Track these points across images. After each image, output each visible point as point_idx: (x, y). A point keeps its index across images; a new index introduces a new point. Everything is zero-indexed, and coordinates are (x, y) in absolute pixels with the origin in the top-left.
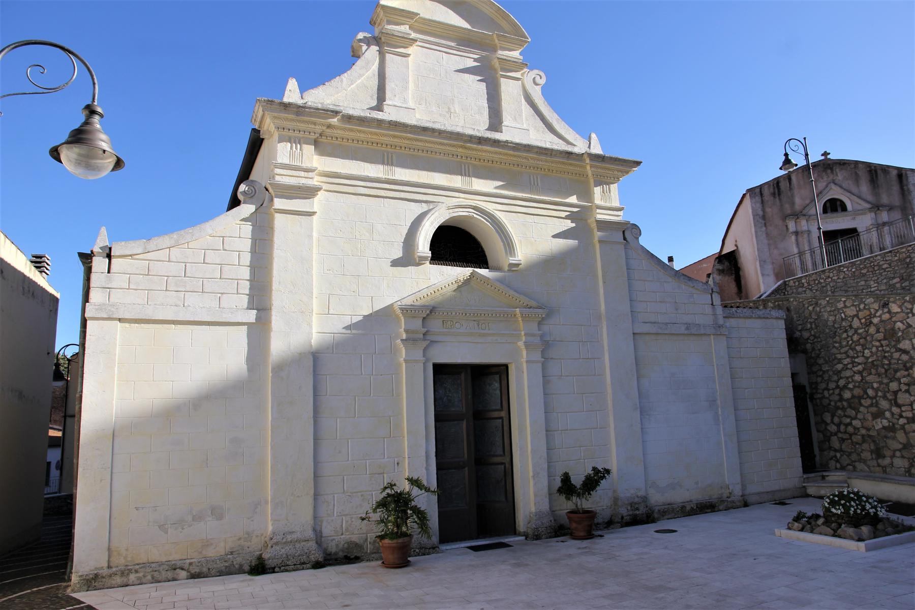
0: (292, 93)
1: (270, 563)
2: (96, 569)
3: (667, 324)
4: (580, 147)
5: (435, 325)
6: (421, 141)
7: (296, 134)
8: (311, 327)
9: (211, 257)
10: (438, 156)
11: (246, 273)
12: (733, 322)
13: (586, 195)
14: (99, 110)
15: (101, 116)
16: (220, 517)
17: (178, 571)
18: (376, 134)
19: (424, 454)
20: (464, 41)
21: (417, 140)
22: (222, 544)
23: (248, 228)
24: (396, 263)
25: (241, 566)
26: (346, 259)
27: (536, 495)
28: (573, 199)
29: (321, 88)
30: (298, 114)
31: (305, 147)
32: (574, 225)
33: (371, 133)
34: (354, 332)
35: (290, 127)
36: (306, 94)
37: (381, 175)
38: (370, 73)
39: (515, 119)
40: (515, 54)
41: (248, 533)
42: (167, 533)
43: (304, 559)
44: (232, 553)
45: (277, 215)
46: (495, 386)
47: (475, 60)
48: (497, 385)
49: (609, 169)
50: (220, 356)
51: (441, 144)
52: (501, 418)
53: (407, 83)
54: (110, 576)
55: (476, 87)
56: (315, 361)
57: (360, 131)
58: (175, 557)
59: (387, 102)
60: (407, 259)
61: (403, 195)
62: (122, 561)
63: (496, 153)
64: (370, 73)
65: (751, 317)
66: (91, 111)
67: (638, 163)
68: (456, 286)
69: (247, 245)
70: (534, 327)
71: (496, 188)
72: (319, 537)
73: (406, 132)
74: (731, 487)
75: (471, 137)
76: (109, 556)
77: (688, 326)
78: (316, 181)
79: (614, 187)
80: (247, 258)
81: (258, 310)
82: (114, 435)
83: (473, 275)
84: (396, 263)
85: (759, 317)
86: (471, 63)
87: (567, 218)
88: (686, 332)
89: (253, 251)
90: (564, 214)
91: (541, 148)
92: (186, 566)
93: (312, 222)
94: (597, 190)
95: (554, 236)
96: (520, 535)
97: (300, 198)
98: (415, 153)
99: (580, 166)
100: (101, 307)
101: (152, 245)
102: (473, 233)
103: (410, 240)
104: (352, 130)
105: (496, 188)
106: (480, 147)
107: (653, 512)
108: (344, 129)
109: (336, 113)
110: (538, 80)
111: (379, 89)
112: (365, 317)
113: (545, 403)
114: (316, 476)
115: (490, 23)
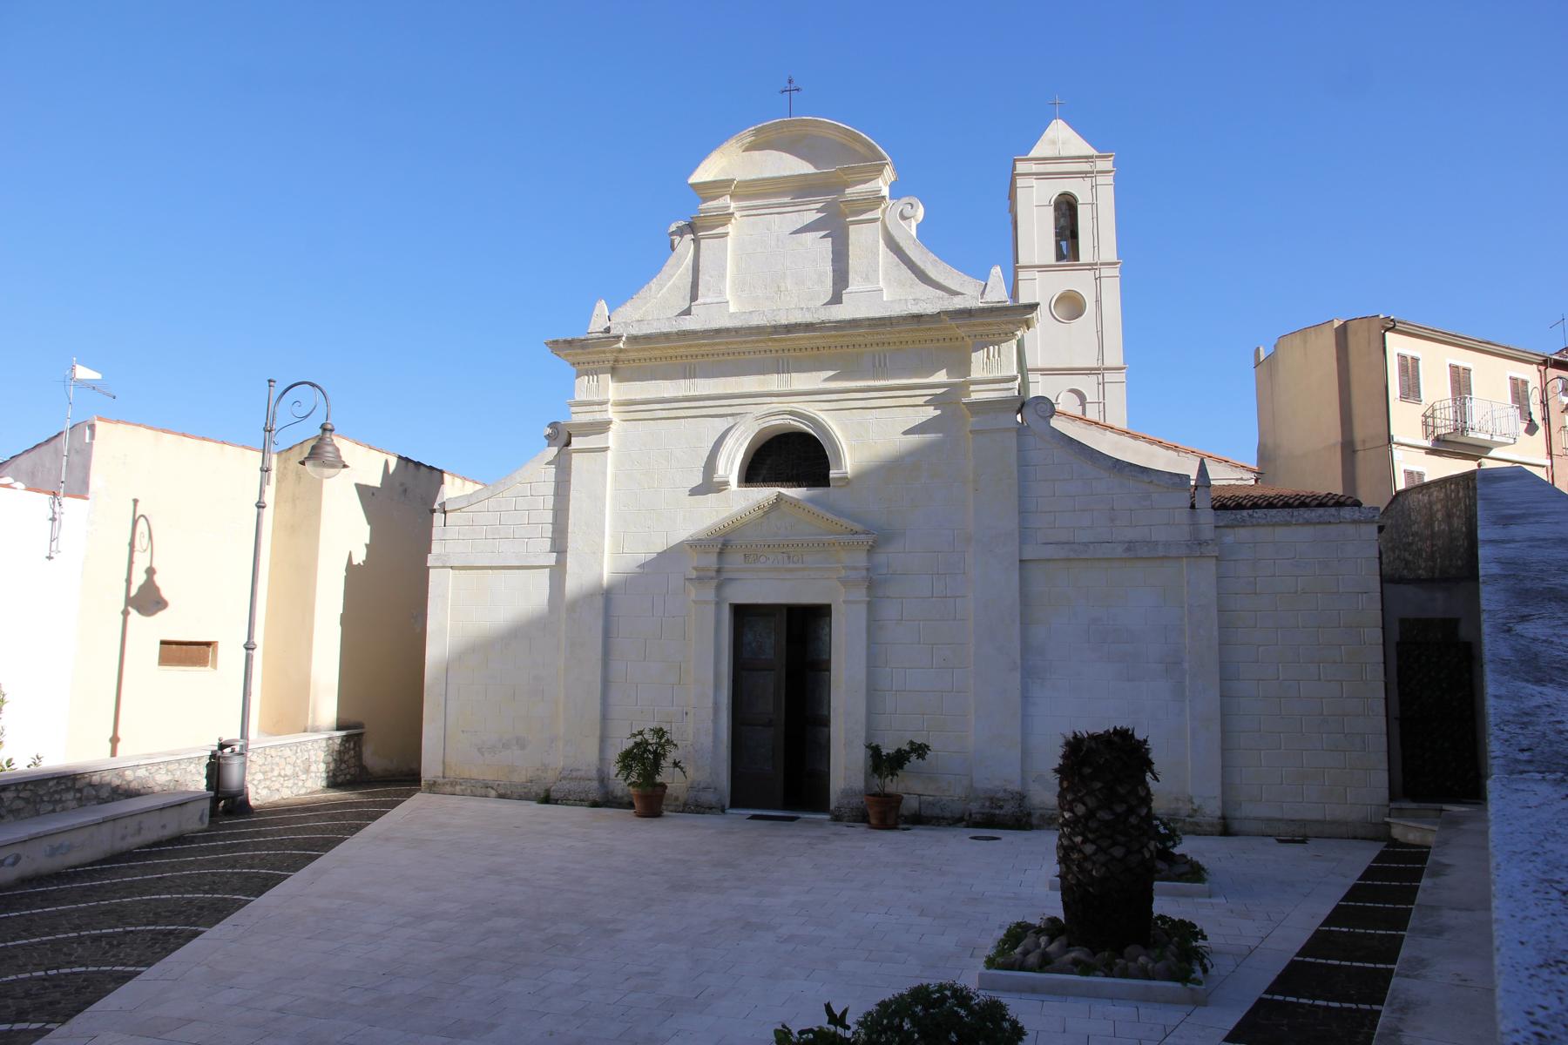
0: (600, 318)
1: (554, 795)
3: (1085, 544)
5: (735, 560)
10: (747, 356)
12: (1230, 537)
13: (963, 366)
16: (523, 747)
20: (800, 189)
23: (552, 470)
24: (694, 492)
26: (654, 487)
28: (941, 377)
37: (681, 393)
39: (867, 279)
47: (819, 211)
50: (526, 596)
55: (819, 247)
56: (607, 598)
58: (489, 776)
59: (700, 301)
60: (709, 485)
65: (1288, 524)
70: (860, 559)
71: (827, 380)
72: (603, 779)
74: (1197, 802)
77: (1130, 546)
82: (447, 669)
83: (780, 497)
84: (694, 492)
85: (1308, 523)
86: (812, 216)
87: (927, 404)
89: (556, 494)
90: (921, 401)
94: (978, 358)
95: (905, 433)
99: (946, 329)
103: (710, 465)
105: (827, 380)
107: (1029, 815)
108: (637, 350)
110: (908, 211)
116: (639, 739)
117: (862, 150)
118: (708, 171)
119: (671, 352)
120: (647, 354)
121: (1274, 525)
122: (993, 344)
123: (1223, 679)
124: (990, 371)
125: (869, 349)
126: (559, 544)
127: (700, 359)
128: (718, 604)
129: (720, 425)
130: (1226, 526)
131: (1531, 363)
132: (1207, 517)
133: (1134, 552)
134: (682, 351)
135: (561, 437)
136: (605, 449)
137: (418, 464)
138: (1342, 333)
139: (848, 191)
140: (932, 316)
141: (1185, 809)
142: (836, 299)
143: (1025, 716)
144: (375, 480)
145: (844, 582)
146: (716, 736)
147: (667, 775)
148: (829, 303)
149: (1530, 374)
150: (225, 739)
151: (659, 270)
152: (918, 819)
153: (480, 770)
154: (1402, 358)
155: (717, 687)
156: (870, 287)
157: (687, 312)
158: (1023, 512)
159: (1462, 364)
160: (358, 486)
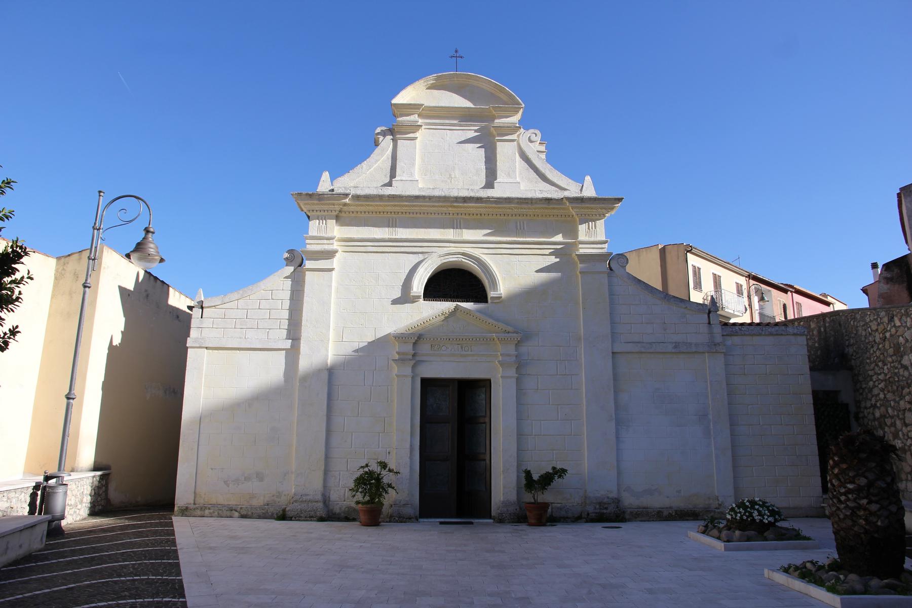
0: (325, 184)
1: (289, 514)
3: (651, 343)
4: (573, 190)
5: (424, 348)
7: (322, 213)
8: (327, 351)
9: (264, 304)
10: (433, 216)
11: (286, 314)
12: (730, 341)
13: (574, 233)
14: (152, 230)
15: (153, 233)
19: (408, 446)
20: (465, 117)
23: (289, 282)
24: (395, 302)
25: (273, 514)
26: (361, 299)
27: (504, 487)
28: (559, 238)
29: (346, 175)
30: (320, 199)
32: (558, 260)
37: (386, 236)
39: (509, 175)
40: (515, 119)
43: (312, 513)
47: (476, 131)
48: (483, 396)
50: (267, 371)
51: (434, 206)
52: (485, 423)
55: (477, 153)
56: (330, 374)
57: (368, 205)
58: (233, 502)
60: (405, 298)
61: (403, 249)
63: (482, 207)
65: (760, 335)
67: (620, 200)
68: (443, 317)
69: (288, 294)
70: (511, 349)
71: (485, 235)
72: (326, 501)
75: (456, 198)
77: (676, 345)
78: (336, 246)
79: (601, 223)
80: (287, 304)
83: (457, 308)
84: (395, 302)
85: (771, 334)
87: (551, 254)
89: (292, 299)
91: (521, 199)
93: (331, 278)
94: (582, 228)
95: (537, 271)
96: (490, 517)
98: (415, 215)
99: (564, 209)
100: (196, 340)
101: (227, 300)
104: (362, 205)
105: (485, 235)
107: (624, 512)
108: (357, 205)
109: (347, 195)
110: (533, 138)
112: (369, 343)
113: (518, 412)
114: (327, 457)
115: (491, 97)
116: (366, 469)
117: (505, 98)
118: (404, 97)
121: (754, 335)
122: (592, 220)
123: (732, 425)
124: (593, 237)
125: (514, 217)
128: (413, 378)
132: (717, 330)
133: (680, 349)
134: (389, 209)
135: (297, 260)
136: (331, 270)
137: (156, 278)
138: (663, 251)
139: (497, 121)
140: (557, 200)
142: (489, 185)
144: (131, 286)
145: (502, 364)
147: (389, 498)
148: (485, 187)
149: (742, 281)
150: (49, 473)
151: (369, 156)
152: (553, 520)
156: (511, 180)
157: (389, 184)
158: (613, 323)
159: (718, 273)
160: (120, 287)
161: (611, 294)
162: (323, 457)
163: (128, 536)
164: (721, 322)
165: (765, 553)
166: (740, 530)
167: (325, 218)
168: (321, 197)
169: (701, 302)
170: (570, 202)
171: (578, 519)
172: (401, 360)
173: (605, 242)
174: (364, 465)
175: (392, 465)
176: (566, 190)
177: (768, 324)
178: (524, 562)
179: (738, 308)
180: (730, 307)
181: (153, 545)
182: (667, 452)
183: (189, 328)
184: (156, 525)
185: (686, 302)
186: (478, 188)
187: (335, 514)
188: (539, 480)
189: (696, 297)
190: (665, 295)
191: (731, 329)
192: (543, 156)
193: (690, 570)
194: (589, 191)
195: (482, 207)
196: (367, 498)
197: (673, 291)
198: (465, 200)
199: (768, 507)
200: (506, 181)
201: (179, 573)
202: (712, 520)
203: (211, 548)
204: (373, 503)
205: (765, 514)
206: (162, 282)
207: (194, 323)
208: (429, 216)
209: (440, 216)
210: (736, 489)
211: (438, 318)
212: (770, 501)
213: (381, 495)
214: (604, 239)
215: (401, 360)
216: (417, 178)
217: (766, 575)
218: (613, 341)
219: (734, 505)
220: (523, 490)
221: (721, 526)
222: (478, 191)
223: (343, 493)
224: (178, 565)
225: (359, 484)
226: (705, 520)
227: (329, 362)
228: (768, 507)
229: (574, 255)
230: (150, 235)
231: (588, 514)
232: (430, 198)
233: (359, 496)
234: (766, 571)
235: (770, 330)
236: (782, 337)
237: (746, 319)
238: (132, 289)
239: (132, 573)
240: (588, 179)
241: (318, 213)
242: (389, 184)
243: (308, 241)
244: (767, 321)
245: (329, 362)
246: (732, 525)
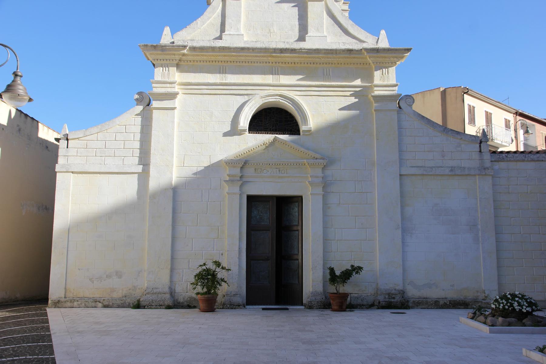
0: (166, 38)
1: (143, 303)
2: (59, 298)
3: (432, 168)
4: (370, 42)
5: (249, 171)
6: (242, 56)
7: (165, 62)
8: (172, 174)
9: (119, 137)
10: (256, 64)
11: (137, 145)
12: (497, 166)
13: (369, 77)
14: (19, 74)
15: (21, 76)
17: (98, 303)
18: (213, 56)
19: (237, 249)
21: (240, 56)
22: (121, 291)
23: (139, 119)
24: (226, 134)
25: (129, 304)
26: (199, 132)
27: (313, 281)
28: (358, 82)
29: (184, 30)
31: (170, 68)
32: (357, 100)
33: (210, 56)
34: (198, 176)
35: (161, 58)
36: (175, 36)
37: (218, 81)
38: (215, 15)
39: (318, 30)
41: (134, 287)
42: (93, 283)
43: (161, 303)
44: (125, 296)
45: (154, 111)
46: (295, 210)
48: (297, 209)
49: (385, 57)
50: (125, 190)
51: (256, 56)
52: (298, 230)
53: (240, 17)
54: (65, 302)
56: (175, 192)
57: (203, 55)
58: (97, 295)
59: (226, 33)
60: (234, 131)
61: (232, 92)
62: (71, 295)
64: (215, 15)
65: (523, 161)
66: (16, 75)
67: (409, 50)
68: (264, 147)
69: (138, 129)
70: (319, 172)
72: (172, 293)
73: (231, 52)
74: (487, 293)
76: (65, 292)
77: (452, 169)
78: (177, 89)
79: (392, 70)
80: (138, 137)
81: (143, 165)
83: (275, 139)
84: (226, 134)
85: (533, 160)
87: (351, 95)
88: (450, 173)
89: (142, 132)
90: (348, 94)
91: (327, 50)
92: (102, 301)
93: (174, 113)
94: (377, 74)
95: (340, 109)
96: (302, 304)
97: (167, 100)
98: (241, 64)
101: (88, 133)
102: (289, 111)
104: (198, 55)
106: (282, 55)
107: (408, 301)
109: (185, 47)
111: (221, 25)
112: (205, 167)
114: (173, 258)
116: (204, 267)
119: (213, 58)
120: (199, 58)
121: (518, 161)
122: (385, 68)
124: (386, 81)
126: (144, 158)
127: (229, 64)
128: (240, 195)
129: (241, 100)
130: (495, 161)
131: (511, 113)
132: (487, 157)
133: (455, 172)
134: (220, 58)
135: (145, 101)
136: (174, 109)
137: (26, 115)
140: (357, 51)
141: (481, 296)
142: (302, 38)
143: (404, 252)
145: (311, 184)
146: (240, 266)
147: (222, 290)
148: (297, 41)
149: (511, 117)
152: (352, 307)
153: (90, 291)
154: (469, 106)
155: (240, 239)
156: (319, 34)
157: (220, 38)
158: (401, 151)
159: (489, 111)
161: (400, 128)
162: (170, 258)
163: (9, 325)
164: (490, 151)
165: (524, 336)
166: (503, 317)
167: (168, 66)
168: (163, 48)
169: (474, 134)
170: (368, 53)
171: (371, 306)
172: (231, 181)
173: (395, 86)
174: (202, 264)
175: (224, 264)
176: (364, 42)
177: (531, 152)
178: (329, 339)
179: (505, 139)
180: (498, 138)
181: (30, 331)
182: (441, 250)
183: (56, 156)
184: (33, 315)
185: (461, 134)
186: (292, 41)
187: (179, 303)
188: (340, 275)
189: (470, 130)
190: (444, 129)
191: (498, 155)
192: (347, 14)
193: (461, 347)
194: (384, 43)
195: (295, 57)
196: (205, 290)
197: (450, 126)
198: (282, 51)
199: (526, 300)
200: (315, 35)
201: (52, 353)
202: (479, 309)
203: (79, 332)
204: (209, 293)
205: (524, 305)
206: (32, 118)
207: (61, 152)
208: (253, 64)
209: (261, 64)
210: (500, 284)
211: (261, 148)
212: (528, 294)
213: (216, 287)
214: (394, 82)
215: (231, 181)
216: (242, 32)
217: (524, 353)
218: (401, 166)
219: (498, 297)
220: (328, 283)
221: (487, 313)
222: (292, 43)
223: (186, 287)
224: (51, 346)
225: (199, 278)
226: (474, 308)
227: (173, 183)
228: (526, 300)
229: (370, 96)
230: (18, 78)
231: (379, 302)
232: (253, 50)
233: (199, 289)
234: (524, 350)
235: (532, 156)
236: (543, 163)
237: (513, 148)
238: (6, 125)
239: (12, 354)
240: (383, 32)
241: (162, 62)
242: (220, 38)
243: (154, 85)
244: (530, 149)
245: (173, 183)
246: (495, 313)
